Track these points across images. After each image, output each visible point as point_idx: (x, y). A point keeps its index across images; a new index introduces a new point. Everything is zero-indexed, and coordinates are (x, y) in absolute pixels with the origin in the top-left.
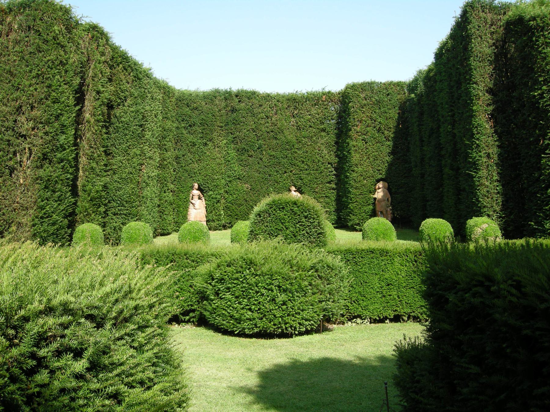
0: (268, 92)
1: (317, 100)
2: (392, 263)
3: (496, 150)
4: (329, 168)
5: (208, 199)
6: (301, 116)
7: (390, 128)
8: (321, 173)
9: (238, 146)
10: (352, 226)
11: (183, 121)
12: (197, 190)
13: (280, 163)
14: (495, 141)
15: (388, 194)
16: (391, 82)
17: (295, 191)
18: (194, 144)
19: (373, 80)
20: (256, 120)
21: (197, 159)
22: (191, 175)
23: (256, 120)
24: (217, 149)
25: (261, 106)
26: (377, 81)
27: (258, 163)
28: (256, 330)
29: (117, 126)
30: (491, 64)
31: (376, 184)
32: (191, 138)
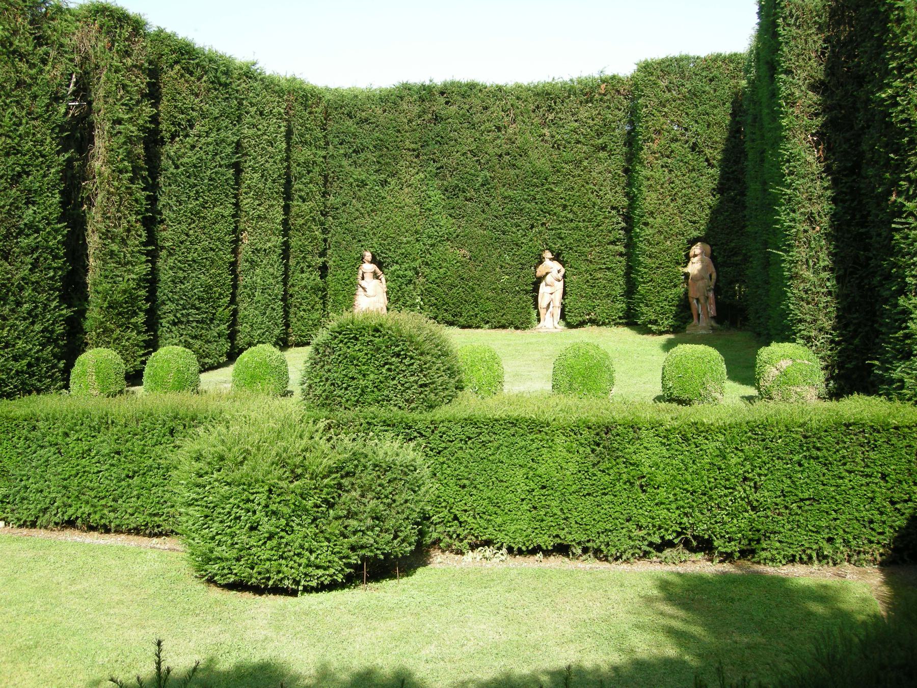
0: (501, 83)
1: (588, 93)
2: (550, 447)
3: (827, 206)
4: (612, 217)
5: (394, 278)
6: (561, 123)
7: (717, 142)
8: (598, 225)
9: (445, 183)
10: (644, 324)
11: (341, 144)
12: (371, 262)
13: (521, 210)
14: (826, 189)
15: (712, 266)
16: (719, 55)
17: (550, 259)
18: (363, 184)
19: (683, 53)
20: (478, 135)
21: (369, 210)
22: (359, 237)
23: (478, 135)
24: (406, 190)
25: (486, 108)
26: (691, 54)
27: (483, 211)
28: (232, 579)
29: (172, 173)
30: (820, 29)
31: (690, 248)
32: (359, 173)
